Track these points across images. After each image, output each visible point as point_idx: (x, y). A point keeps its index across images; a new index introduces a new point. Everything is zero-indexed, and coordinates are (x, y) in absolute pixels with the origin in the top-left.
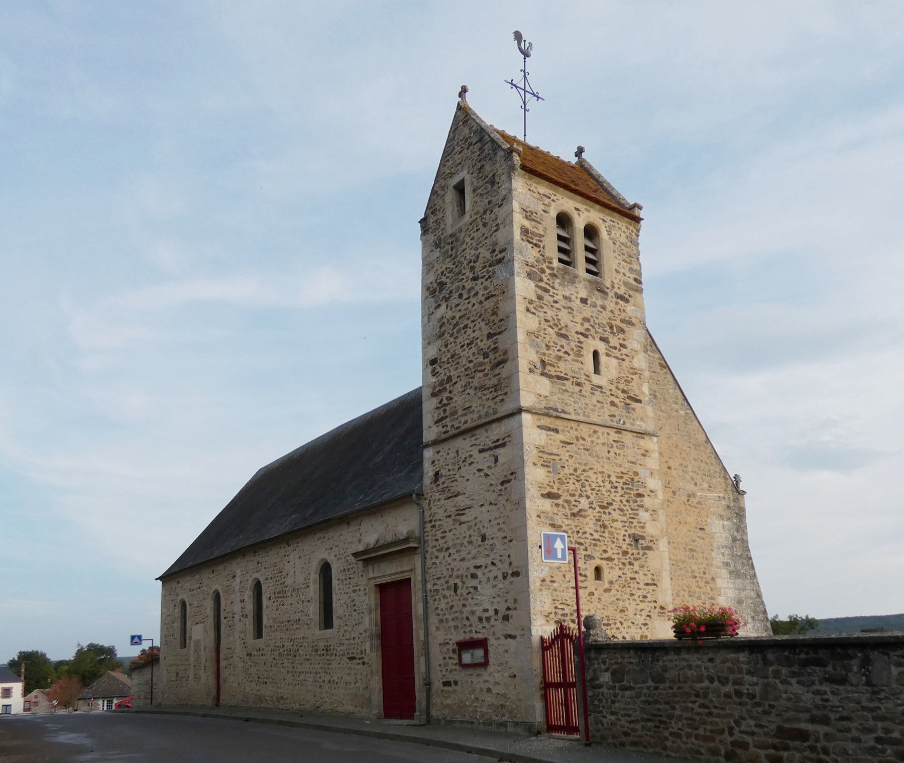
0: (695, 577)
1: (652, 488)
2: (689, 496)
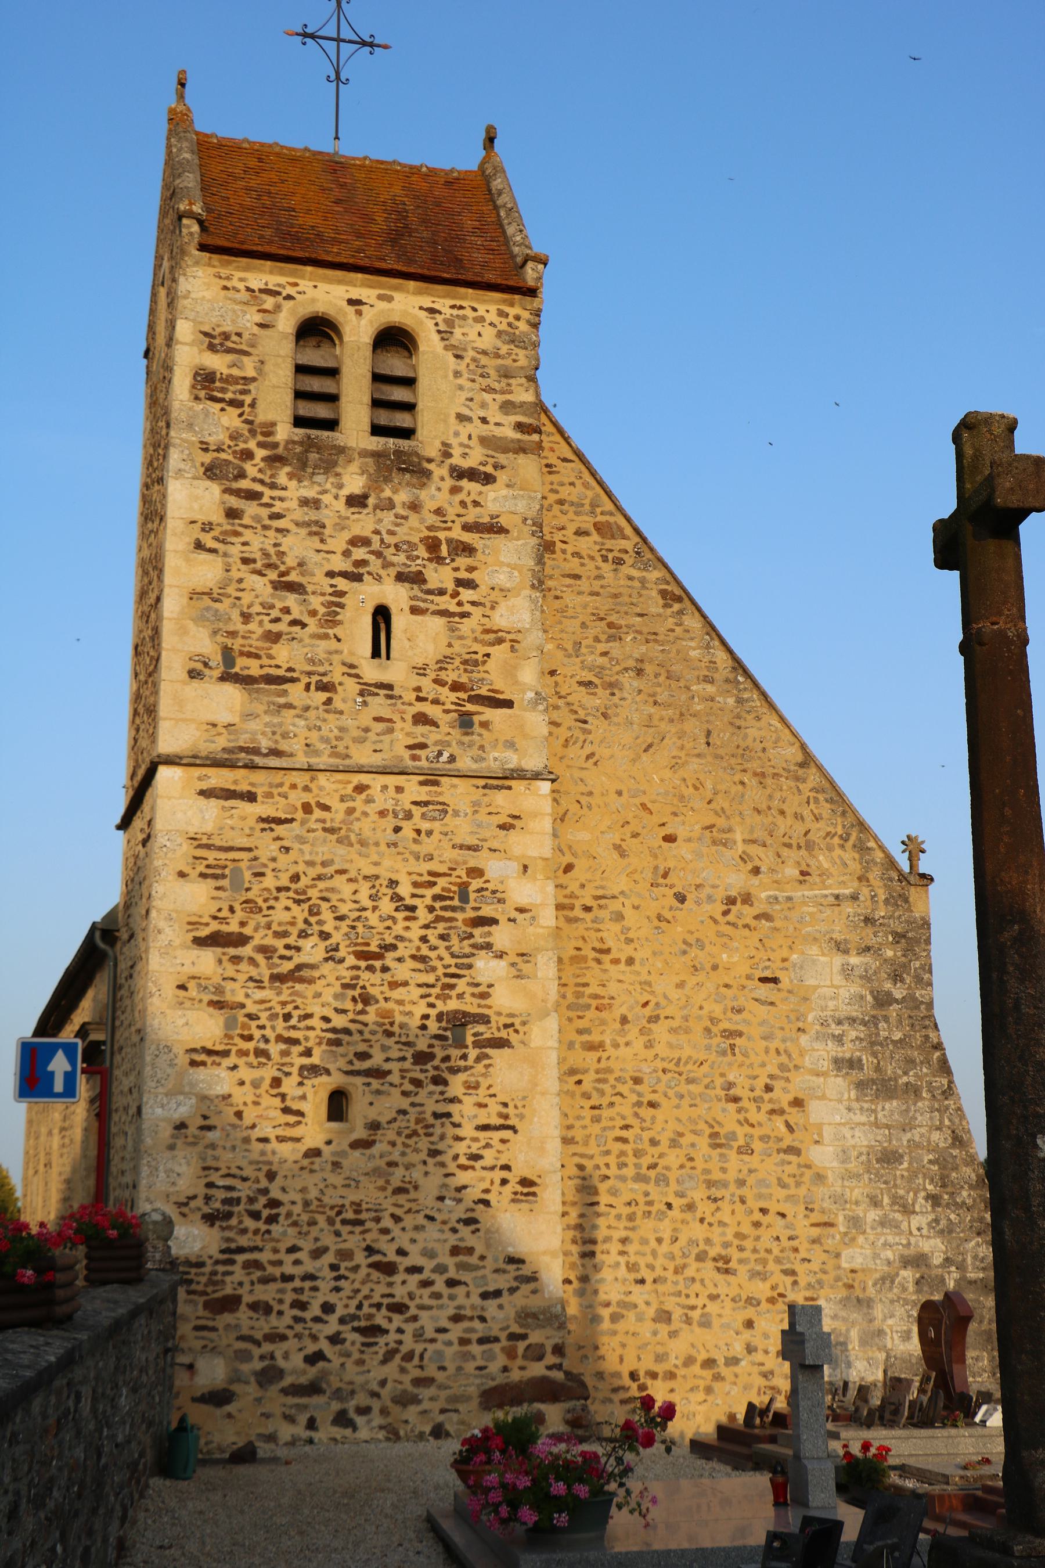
0: (736, 1100)
1: (523, 901)
2: (731, 901)
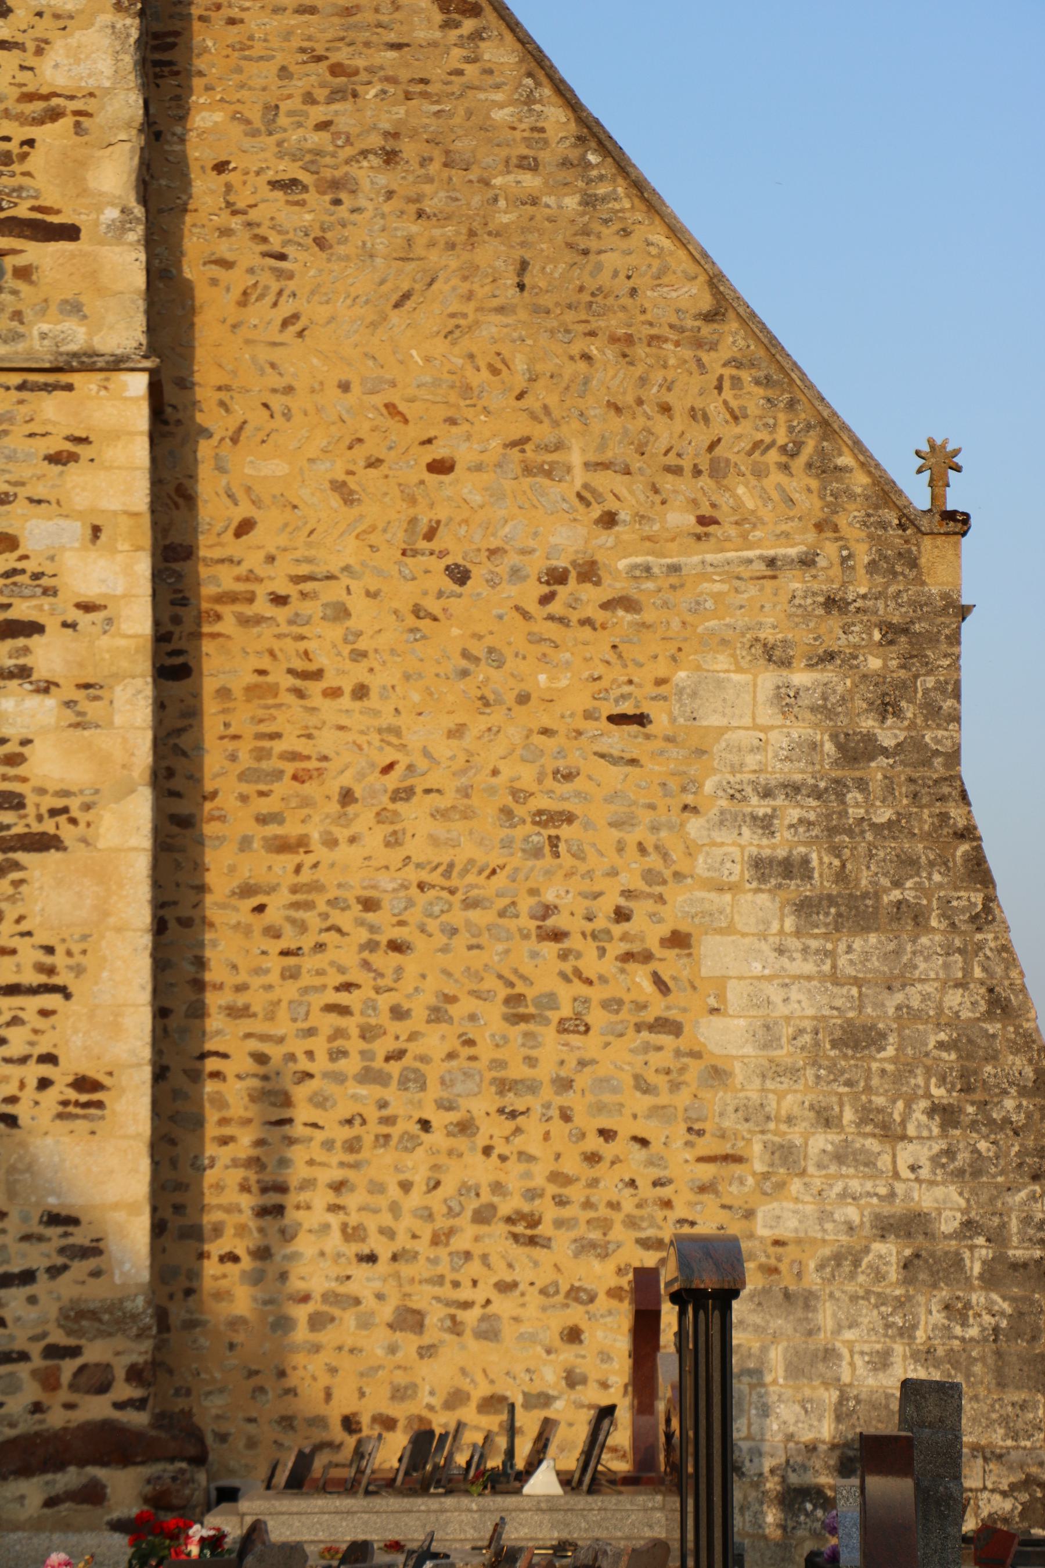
0: (558, 936)
1: (91, 591)
